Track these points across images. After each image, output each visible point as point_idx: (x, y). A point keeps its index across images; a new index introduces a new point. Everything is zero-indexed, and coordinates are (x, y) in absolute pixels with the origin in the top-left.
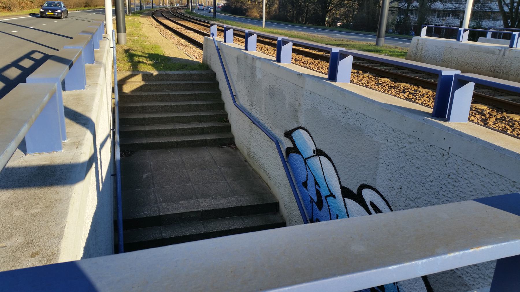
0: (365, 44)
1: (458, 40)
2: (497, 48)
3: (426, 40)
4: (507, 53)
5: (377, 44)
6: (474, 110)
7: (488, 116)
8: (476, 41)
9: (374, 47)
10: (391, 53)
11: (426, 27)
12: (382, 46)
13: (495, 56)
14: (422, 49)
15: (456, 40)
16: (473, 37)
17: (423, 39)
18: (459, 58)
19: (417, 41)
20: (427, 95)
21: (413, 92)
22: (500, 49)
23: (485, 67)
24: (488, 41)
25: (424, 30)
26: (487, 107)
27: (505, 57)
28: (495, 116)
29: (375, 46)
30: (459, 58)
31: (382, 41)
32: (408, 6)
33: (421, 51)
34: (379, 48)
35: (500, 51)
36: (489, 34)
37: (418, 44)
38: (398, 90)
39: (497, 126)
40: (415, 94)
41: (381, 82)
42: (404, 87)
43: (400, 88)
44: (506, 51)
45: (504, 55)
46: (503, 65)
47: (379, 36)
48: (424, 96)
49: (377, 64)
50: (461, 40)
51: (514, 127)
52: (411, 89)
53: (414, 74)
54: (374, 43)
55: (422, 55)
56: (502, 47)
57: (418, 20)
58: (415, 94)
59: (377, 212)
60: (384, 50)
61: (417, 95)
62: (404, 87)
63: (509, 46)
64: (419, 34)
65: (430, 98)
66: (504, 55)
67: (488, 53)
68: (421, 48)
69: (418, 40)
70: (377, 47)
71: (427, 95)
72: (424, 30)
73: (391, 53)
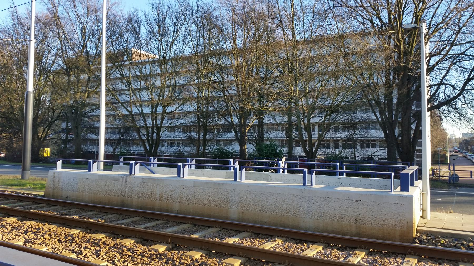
0: (12, 178)
1: (89, 171)
2: (120, 176)
3: (61, 173)
4: (128, 179)
5: (23, 177)
6: (92, 242)
7: (102, 246)
8: (111, 171)
9: (19, 180)
10: (35, 186)
11: (61, 160)
12: (29, 179)
13: (120, 182)
14: (58, 182)
15: (87, 171)
16: (108, 167)
17: (58, 172)
18: (92, 187)
19: (53, 175)
20: (50, 232)
21: (35, 230)
22: (123, 176)
23: (113, 193)
24: (118, 170)
25: (59, 164)
26: (105, 235)
27: (127, 183)
28: (108, 245)
29: (21, 179)
30: (92, 187)
31: (28, 174)
32: (67, 137)
33: (58, 183)
34: (23, 181)
35: (123, 178)
36: (121, 164)
37: (54, 177)
38: (20, 231)
39: (107, 257)
40: (37, 233)
41: (6, 223)
42: (28, 227)
43: (23, 228)
44: (127, 178)
45: (126, 181)
46: (127, 190)
47: (24, 170)
48: (46, 234)
49: (14, 201)
50: (91, 171)
51: (122, 253)
52: (34, 227)
53: (50, 207)
54: (19, 176)
55: (59, 187)
56: (124, 175)
57: (44, 157)
58: (37, 233)
59: (452, 211)
60: (28, 183)
61: (40, 233)
62: (28, 227)
63: (129, 173)
64: (55, 167)
65: (52, 235)
66: (126, 181)
67: (114, 180)
68: (57, 180)
69: (54, 173)
70: (22, 180)
71: (50, 232)
72: (59, 164)
73: (35, 186)
